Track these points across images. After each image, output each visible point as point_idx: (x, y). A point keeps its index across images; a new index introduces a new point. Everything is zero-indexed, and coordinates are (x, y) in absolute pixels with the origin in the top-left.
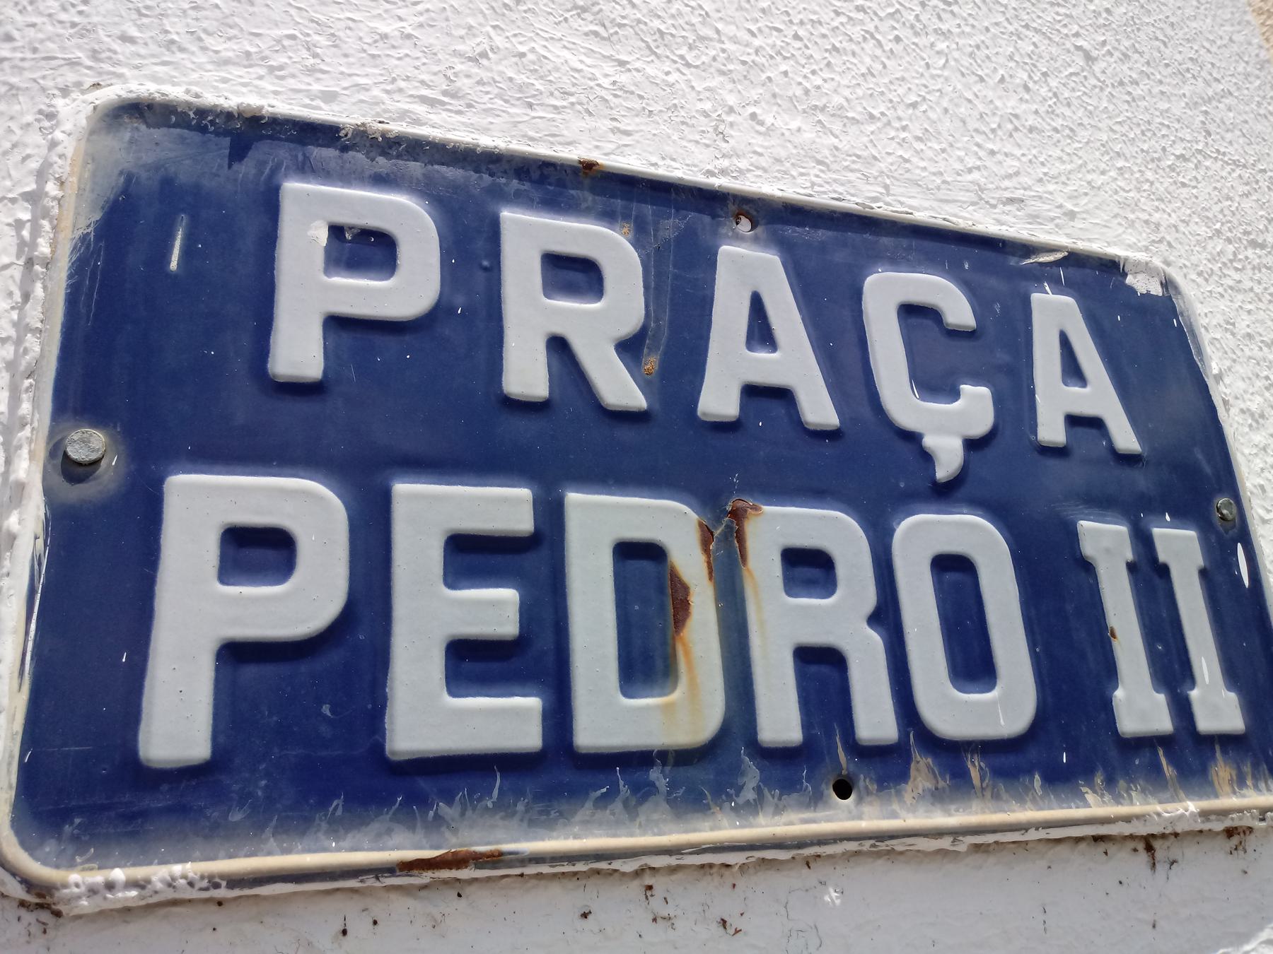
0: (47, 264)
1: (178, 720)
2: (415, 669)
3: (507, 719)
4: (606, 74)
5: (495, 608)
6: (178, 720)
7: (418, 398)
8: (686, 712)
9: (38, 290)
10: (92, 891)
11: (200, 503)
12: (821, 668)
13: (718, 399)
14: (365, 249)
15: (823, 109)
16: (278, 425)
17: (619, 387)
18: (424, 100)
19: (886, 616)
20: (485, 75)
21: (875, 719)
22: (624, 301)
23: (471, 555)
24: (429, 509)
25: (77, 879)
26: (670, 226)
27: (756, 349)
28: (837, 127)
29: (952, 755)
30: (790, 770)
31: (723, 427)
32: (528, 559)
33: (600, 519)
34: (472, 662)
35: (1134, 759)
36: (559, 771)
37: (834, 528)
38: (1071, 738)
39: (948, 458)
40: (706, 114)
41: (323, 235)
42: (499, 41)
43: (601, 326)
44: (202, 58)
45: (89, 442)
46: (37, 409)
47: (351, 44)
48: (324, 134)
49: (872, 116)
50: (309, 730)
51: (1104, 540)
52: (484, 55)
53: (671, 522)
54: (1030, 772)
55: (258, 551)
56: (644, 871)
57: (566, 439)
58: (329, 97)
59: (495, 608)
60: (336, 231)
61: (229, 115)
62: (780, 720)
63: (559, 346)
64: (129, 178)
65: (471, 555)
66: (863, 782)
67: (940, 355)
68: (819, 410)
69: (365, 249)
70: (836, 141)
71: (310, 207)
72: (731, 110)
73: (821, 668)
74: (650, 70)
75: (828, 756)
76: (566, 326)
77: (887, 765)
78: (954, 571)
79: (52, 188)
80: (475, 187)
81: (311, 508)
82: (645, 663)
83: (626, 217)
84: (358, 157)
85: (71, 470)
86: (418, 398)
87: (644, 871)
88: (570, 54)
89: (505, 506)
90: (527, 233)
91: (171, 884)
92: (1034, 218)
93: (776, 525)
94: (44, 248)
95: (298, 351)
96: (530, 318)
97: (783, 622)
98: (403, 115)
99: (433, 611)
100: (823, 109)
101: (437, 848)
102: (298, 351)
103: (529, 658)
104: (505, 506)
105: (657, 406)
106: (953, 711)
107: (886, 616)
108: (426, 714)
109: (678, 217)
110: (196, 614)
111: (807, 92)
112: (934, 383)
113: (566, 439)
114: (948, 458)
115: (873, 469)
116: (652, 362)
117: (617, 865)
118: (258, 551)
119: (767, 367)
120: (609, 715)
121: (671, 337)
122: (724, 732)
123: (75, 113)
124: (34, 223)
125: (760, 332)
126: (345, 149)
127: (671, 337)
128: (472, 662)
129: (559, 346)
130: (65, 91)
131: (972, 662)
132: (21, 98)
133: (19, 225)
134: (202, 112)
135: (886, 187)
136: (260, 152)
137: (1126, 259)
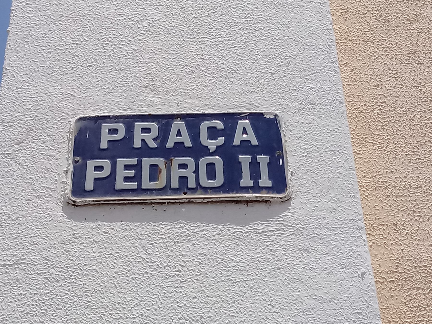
0: (71, 139)
1: (89, 185)
4: (156, 100)
5: (131, 173)
6: (89, 185)
8: (161, 183)
9: (70, 142)
10: (80, 202)
11: (91, 164)
12: (183, 179)
13: (170, 144)
14: (114, 131)
15: (201, 98)
16: (101, 154)
18: (124, 110)
19: (196, 172)
20: (134, 104)
21: (192, 183)
22: (155, 132)
23: (127, 167)
24: (121, 162)
25: (78, 200)
26: (164, 121)
28: (203, 100)
29: (206, 190)
30: (175, 191)
31: (104, 150)
32: (138, 167)
33: (147, 162)
34: (127, 179)
36: (139, 190)
37: (190, 161)
40: (175, 103)
41: (108, 130)
42: (137, 99)
44: (90, 110)
45: (77, 159)
46: (71, 155)
47: (112, 104)
48: (108, 117)
49: (212, 97)
50: (106, 185)
51: (245, 159)
52: (135, 101)
53: (160, 161)
54: (220, 191)
55: (99, 168)
58: (109, 112)
59: (131, 173)
60: (109, 130)
61: (94, 117)
62: (175, 184)
63: (143, 140)
64: (81, 128)
65: (127, 167)
66: (188, 193)
67: (213, 133)
68: (188, 144)
70: (203, 103)
71: (105, 127)
72: (181, 101)
73: (183, 179)
74: (165, 98)
77: (193, 190)
78: (211, 166)
79: (71, 130)
80: (129, 121)
81: (106, 163)
83: (156, 121)
84: (113, 120)
85: (76, 162)
88: (150, 98)
89: (134, 161)
90: (139, 125)
91: (89, 201)
92: (248, 109)
93: (177, 161)
94: (71, 137)
95: (104, 145)
97: (176, 173)
98: (121, 113)
99: (121, 173)
100: (201, 98)
102: (104, 145)
103: (137, 178)
104: (134, 161)
105: (260, 144)
106: (205, 182)
107: (196, 172)
108: (120, 184)
109: (165, 120)
110: (91, 175)
111: (198, 95)
112: (211, 137)
113: (146, 151)
115: (198, 151)
116: (159, 141)
117: (147, 201)
118: (99, 168)
119: (179, 139)
120: (146, 184)
122: (166, 186)
123: (73, 120)
124: (69, 135)
125: (179, 134)
126: (111, 119)
128: (127, 179)
129: (143, 140)
130: (72, 118)
131: (211, 175)
133: (67, 136)
134: (90, 117)
135: (213, 109)
136: (99, 122)
137: (264, 112)
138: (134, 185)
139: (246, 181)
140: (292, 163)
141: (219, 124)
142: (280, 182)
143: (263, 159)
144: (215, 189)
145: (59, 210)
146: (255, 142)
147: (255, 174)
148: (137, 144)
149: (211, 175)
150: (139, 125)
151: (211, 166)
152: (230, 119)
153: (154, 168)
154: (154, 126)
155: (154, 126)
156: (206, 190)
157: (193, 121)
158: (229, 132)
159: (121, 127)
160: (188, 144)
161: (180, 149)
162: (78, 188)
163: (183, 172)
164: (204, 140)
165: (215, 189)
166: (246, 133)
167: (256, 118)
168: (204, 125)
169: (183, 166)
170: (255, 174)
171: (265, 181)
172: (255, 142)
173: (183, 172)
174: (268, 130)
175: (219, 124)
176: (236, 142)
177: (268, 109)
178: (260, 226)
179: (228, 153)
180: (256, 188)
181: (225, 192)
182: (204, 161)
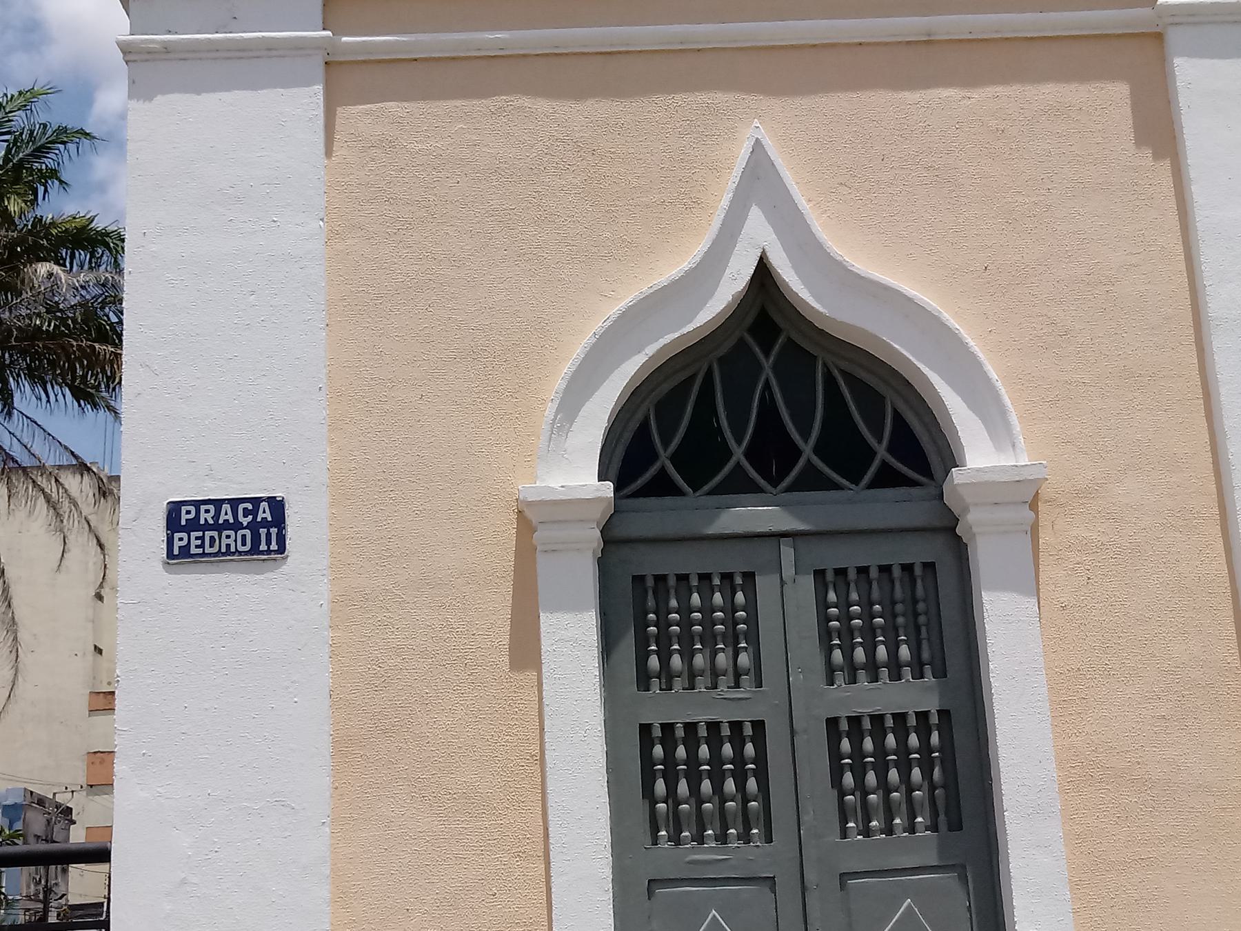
1: (176, 552)
2: (192, 547)
3: (200, 551)
5: (199, 542)
6: (176, 552)
7: (193, 525)
11: (177, 536)
12: (228, 546)
14: (188, 512)
17: (211, 522)
21: (233, 549)
23: (197, 538)
27: (226, 515)
29: (240, 553)
30: (224, 554)
32: (202, 538)
34: (197, 547)
35: (262, 553)
36: (204, 554)
37: (232, 533)
38: (255, 550)
39: (245, 524)
43: (209, 517)
50: (185, 552)
51: (263, 531)
53: (215, 534)
55: (181, 539)
56: (211, 562)
57: (207, 527)
59: (199, 542)
62: (223, 550)
65: (197, 538)
67: (246, 512)
68: (231, 521)
69: (188, 512)
71: (184, 509)
73: (228, 546)
75: (228, 552)
76: (206, 517)
77: (233, 554)
78: (244, 536)
80: (197, 504)
81: (184, 535)
82: (211, 546)
86: (193, 525)
87: (211, 562)
89: (200, 534)
90: (203, 508)
93: (225, 533)
95: (183, 523)
96: (203, 516)
97: (225, 541)
99: (194, 542)
101: (818, 300)
102: (183, 523)
103: (202, 546)
104: (200, 534)
106: (241, 548)
108: (193, 550)
109: (218, 503)
110: (177, 544)
113: (207, 527)
114: (245, 524)
115: (237, 526)
118: (181, 539)
121: (217, 516)
127: (217, 516)
128: (197, 547)
131: (244, 544)
132: (86, 477)
138: (201, 551)
139: (263, 547)
140: (290, 532)
141: (250, 506)
142: (282, 549)
143: (274, 531)
144: (246, 553)
145: (160, 567)
146: (270, 519)
147: (269, 543)
148: (202, 522)
149: (244, 544)
150: (203, 508)
151: (244, 536)
152: (256, 501)
153: (212, 538)
154: (211, 508)
155: (211, 508)
156: (240, 553)
157: (234, 503)
158: (254, 512)
159: (192, 509)
160: (231, 521)
161: (227, 525)
162: (170, 555)
163: (228, 541)
164: (241, 518)
165: (246, 553)
166: (265, 513)
167: (271, 500)
168: (241, 507)
169: (228, 537)
170: (269, 543)
171: (274, 546)
172: (270, 519)
173: (228, 541)
174: (277, 506)
175: (250, 506)
176: (259, 519)
177: (278, 494)
178: (269, 575)
179: (254, 527)
180: (269, 552)
181: (904, 476)
182: (241, 532)
